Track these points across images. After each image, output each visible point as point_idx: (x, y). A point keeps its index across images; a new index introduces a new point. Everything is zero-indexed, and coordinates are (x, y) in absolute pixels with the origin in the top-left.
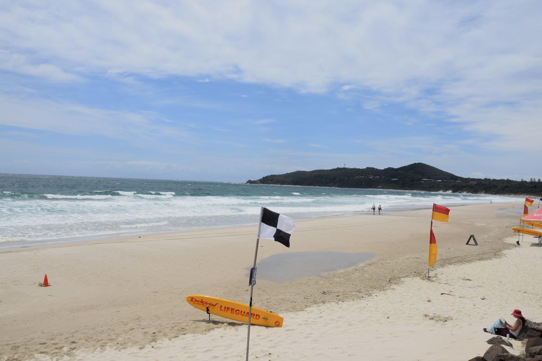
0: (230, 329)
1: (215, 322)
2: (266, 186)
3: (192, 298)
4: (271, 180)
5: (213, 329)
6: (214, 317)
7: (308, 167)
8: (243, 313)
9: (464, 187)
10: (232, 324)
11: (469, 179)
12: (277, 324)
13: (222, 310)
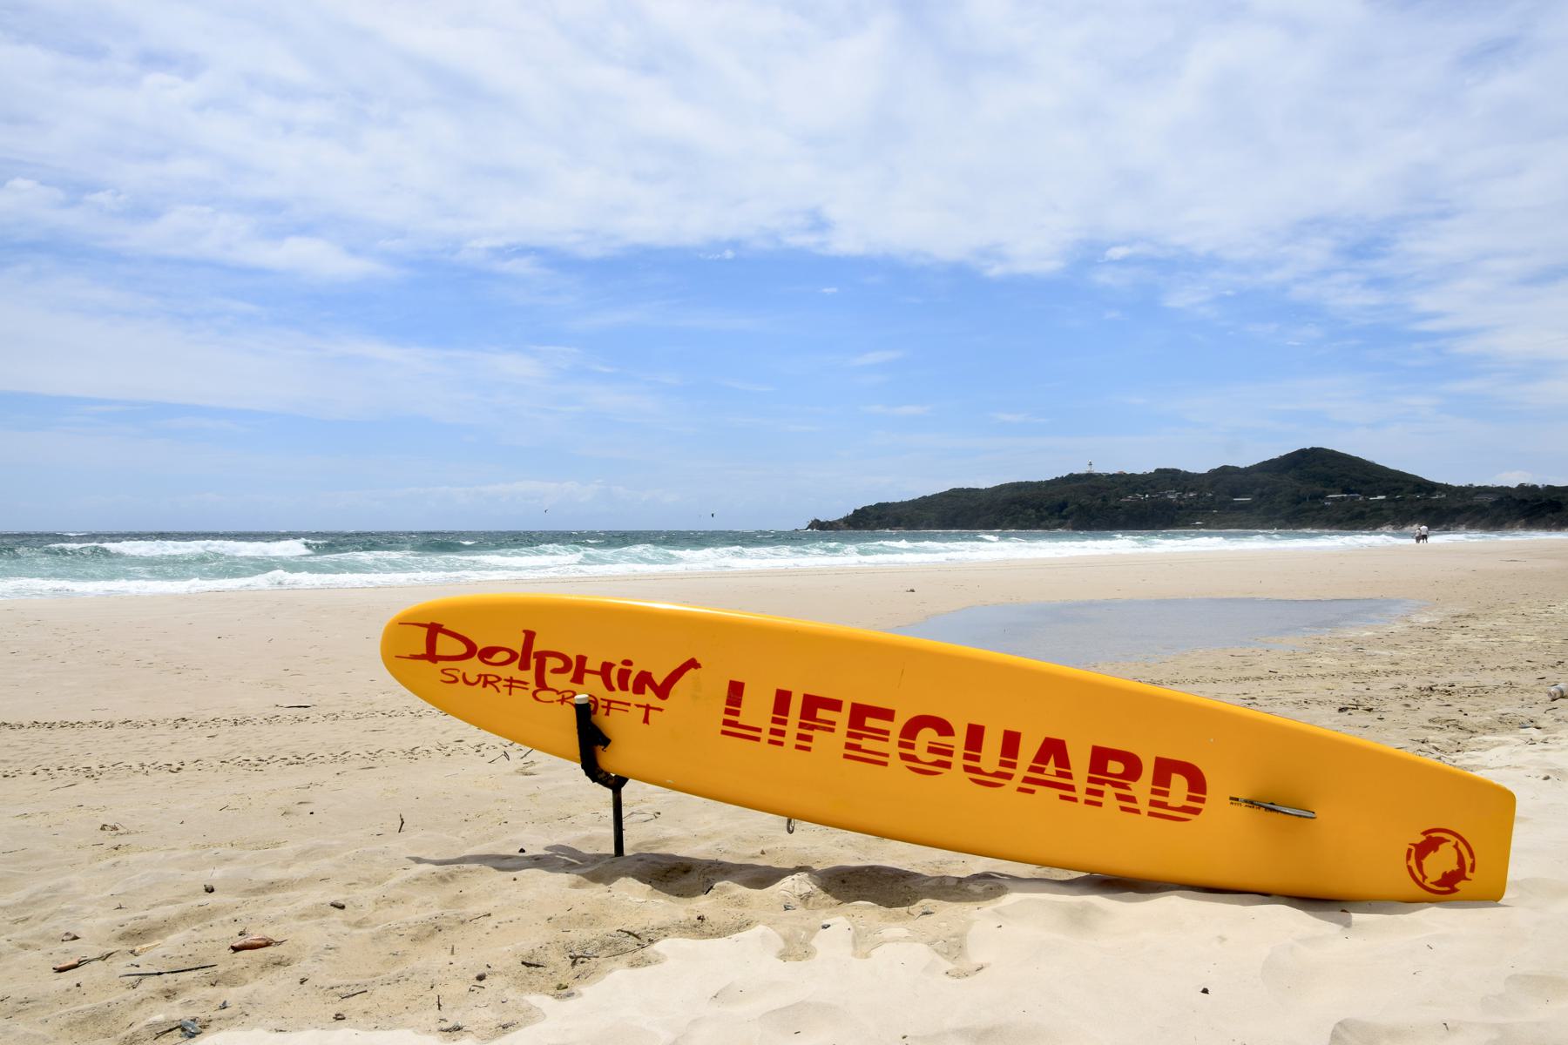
0: (861, 942)
1: (674, 875)
3: (434, 630)
4: (879, 518)
5: (635, 943)
6: (669, 819)
9: (1458, 512)
10: (847, 884)
11: (1470, 488)
12: (1440, 863)
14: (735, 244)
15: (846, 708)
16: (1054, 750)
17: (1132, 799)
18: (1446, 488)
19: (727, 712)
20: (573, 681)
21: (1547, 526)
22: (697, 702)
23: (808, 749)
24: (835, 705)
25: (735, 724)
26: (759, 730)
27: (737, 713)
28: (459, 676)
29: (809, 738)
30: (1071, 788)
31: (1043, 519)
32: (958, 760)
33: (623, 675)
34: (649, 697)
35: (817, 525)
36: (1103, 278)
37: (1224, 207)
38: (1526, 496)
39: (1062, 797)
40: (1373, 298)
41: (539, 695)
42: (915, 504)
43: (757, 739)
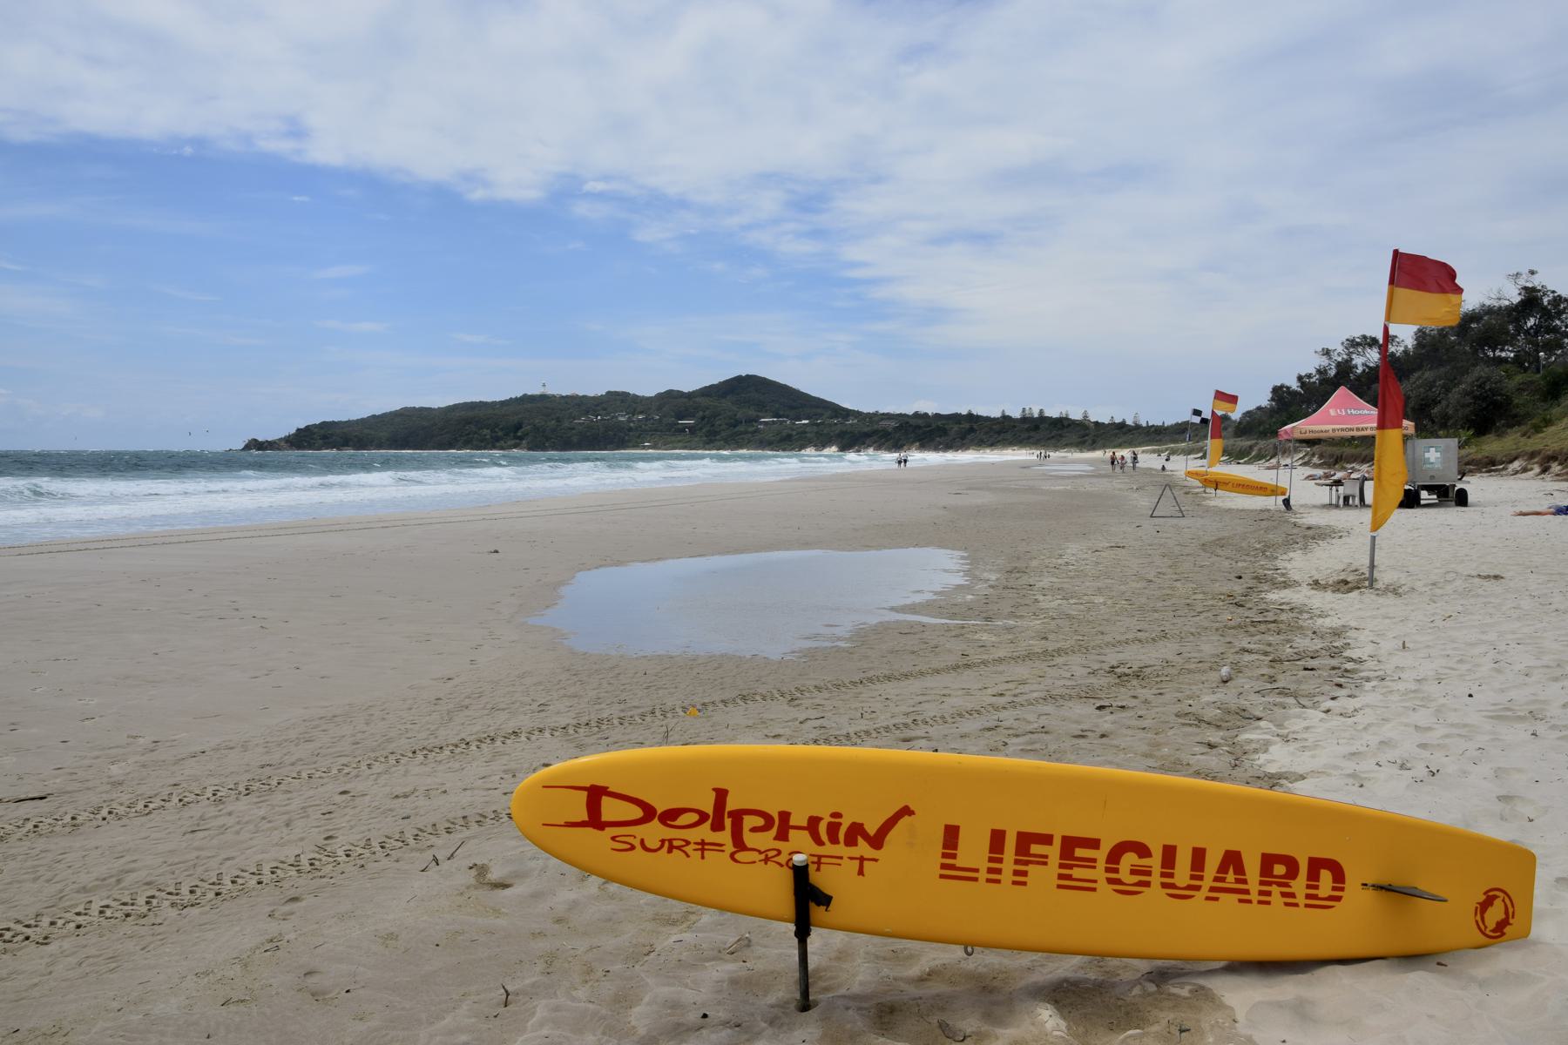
3: (596, 794)
7: (438, 398)
8: (1182, 873)
9: (867, 435)
11: (876, 414)
12: (1495, 914)
13: (969, 875)
14: (199, 142)
15: (1057, 842)
16: (1232, 860)
17: (1292, 895)
18: (857, 414)
19: (944, 856)
20: (776, 838)
21: (936, 449)
22: (911, 851)
23: (1024, 884)
24: (1047, 839)
25: (952, 867)
26: (977, 870)
27: (954, 856)
28: (636, 843)
29: (1025, 874)
30: (1247, 892)
31: (498, 439)
32: (1156, 879)
33: (833, 829)
34: (863, 849)
35: (254, 445)
36: (581, 209)
37: (699, 156)
38: (920, 422)
39: (1241, 901)
40: (807, 247)
41: (737, 856)
43: (976, 879)
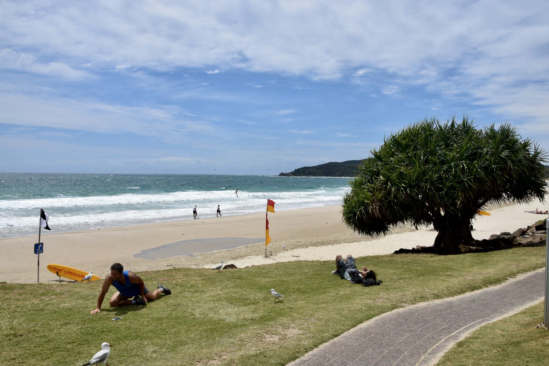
2: (332, 179)
4: (303, 172)
42: (320, 166)
